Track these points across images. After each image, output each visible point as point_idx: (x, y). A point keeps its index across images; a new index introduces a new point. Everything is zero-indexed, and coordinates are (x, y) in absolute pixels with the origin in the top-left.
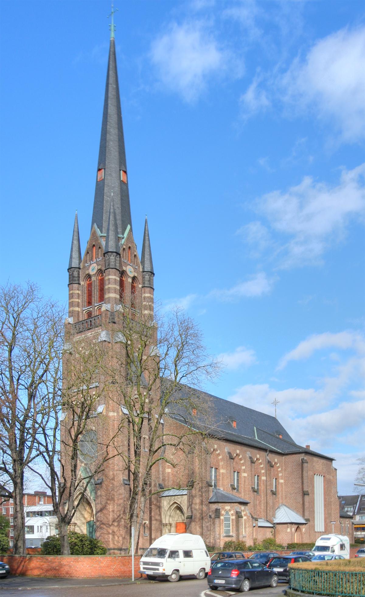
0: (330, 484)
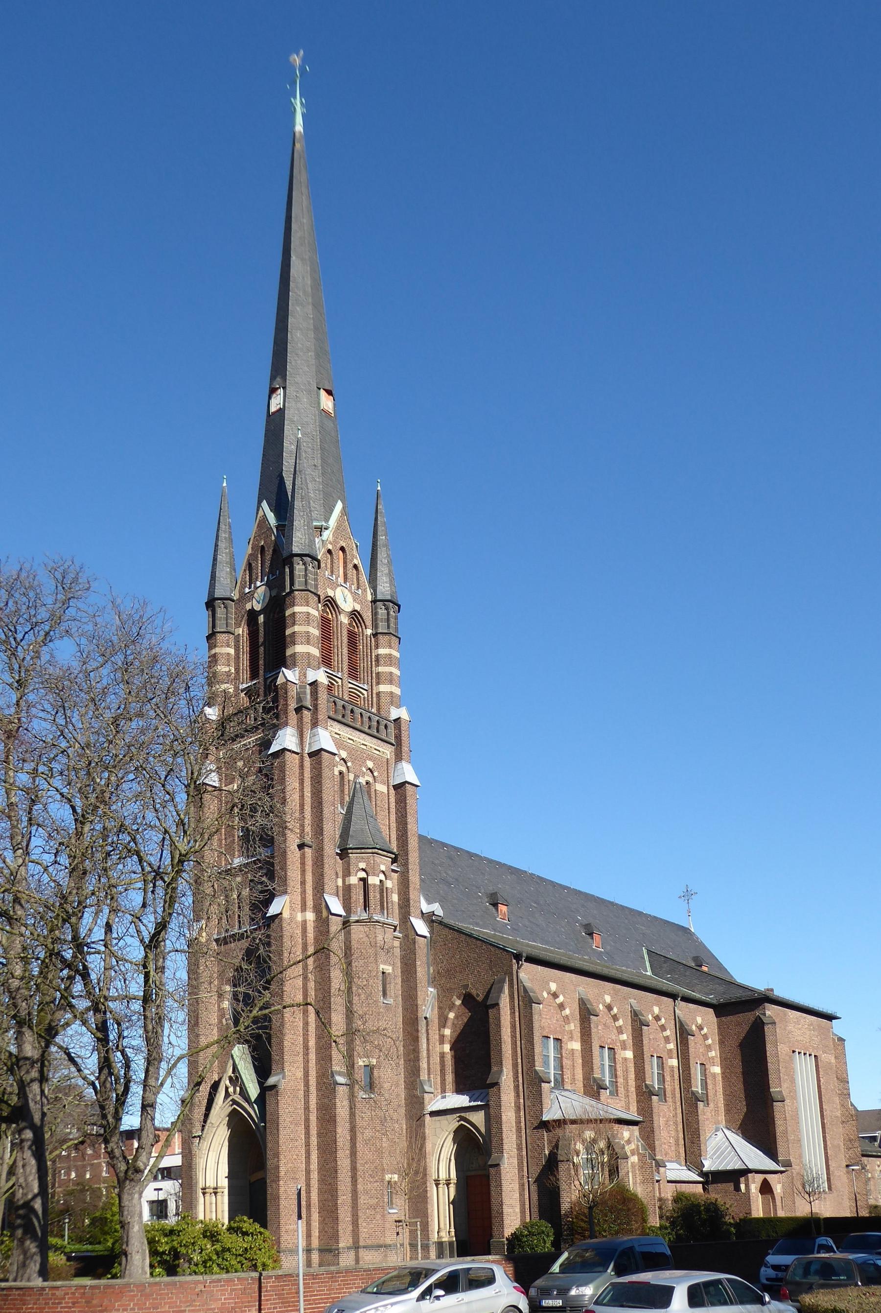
0: (834, 1079)
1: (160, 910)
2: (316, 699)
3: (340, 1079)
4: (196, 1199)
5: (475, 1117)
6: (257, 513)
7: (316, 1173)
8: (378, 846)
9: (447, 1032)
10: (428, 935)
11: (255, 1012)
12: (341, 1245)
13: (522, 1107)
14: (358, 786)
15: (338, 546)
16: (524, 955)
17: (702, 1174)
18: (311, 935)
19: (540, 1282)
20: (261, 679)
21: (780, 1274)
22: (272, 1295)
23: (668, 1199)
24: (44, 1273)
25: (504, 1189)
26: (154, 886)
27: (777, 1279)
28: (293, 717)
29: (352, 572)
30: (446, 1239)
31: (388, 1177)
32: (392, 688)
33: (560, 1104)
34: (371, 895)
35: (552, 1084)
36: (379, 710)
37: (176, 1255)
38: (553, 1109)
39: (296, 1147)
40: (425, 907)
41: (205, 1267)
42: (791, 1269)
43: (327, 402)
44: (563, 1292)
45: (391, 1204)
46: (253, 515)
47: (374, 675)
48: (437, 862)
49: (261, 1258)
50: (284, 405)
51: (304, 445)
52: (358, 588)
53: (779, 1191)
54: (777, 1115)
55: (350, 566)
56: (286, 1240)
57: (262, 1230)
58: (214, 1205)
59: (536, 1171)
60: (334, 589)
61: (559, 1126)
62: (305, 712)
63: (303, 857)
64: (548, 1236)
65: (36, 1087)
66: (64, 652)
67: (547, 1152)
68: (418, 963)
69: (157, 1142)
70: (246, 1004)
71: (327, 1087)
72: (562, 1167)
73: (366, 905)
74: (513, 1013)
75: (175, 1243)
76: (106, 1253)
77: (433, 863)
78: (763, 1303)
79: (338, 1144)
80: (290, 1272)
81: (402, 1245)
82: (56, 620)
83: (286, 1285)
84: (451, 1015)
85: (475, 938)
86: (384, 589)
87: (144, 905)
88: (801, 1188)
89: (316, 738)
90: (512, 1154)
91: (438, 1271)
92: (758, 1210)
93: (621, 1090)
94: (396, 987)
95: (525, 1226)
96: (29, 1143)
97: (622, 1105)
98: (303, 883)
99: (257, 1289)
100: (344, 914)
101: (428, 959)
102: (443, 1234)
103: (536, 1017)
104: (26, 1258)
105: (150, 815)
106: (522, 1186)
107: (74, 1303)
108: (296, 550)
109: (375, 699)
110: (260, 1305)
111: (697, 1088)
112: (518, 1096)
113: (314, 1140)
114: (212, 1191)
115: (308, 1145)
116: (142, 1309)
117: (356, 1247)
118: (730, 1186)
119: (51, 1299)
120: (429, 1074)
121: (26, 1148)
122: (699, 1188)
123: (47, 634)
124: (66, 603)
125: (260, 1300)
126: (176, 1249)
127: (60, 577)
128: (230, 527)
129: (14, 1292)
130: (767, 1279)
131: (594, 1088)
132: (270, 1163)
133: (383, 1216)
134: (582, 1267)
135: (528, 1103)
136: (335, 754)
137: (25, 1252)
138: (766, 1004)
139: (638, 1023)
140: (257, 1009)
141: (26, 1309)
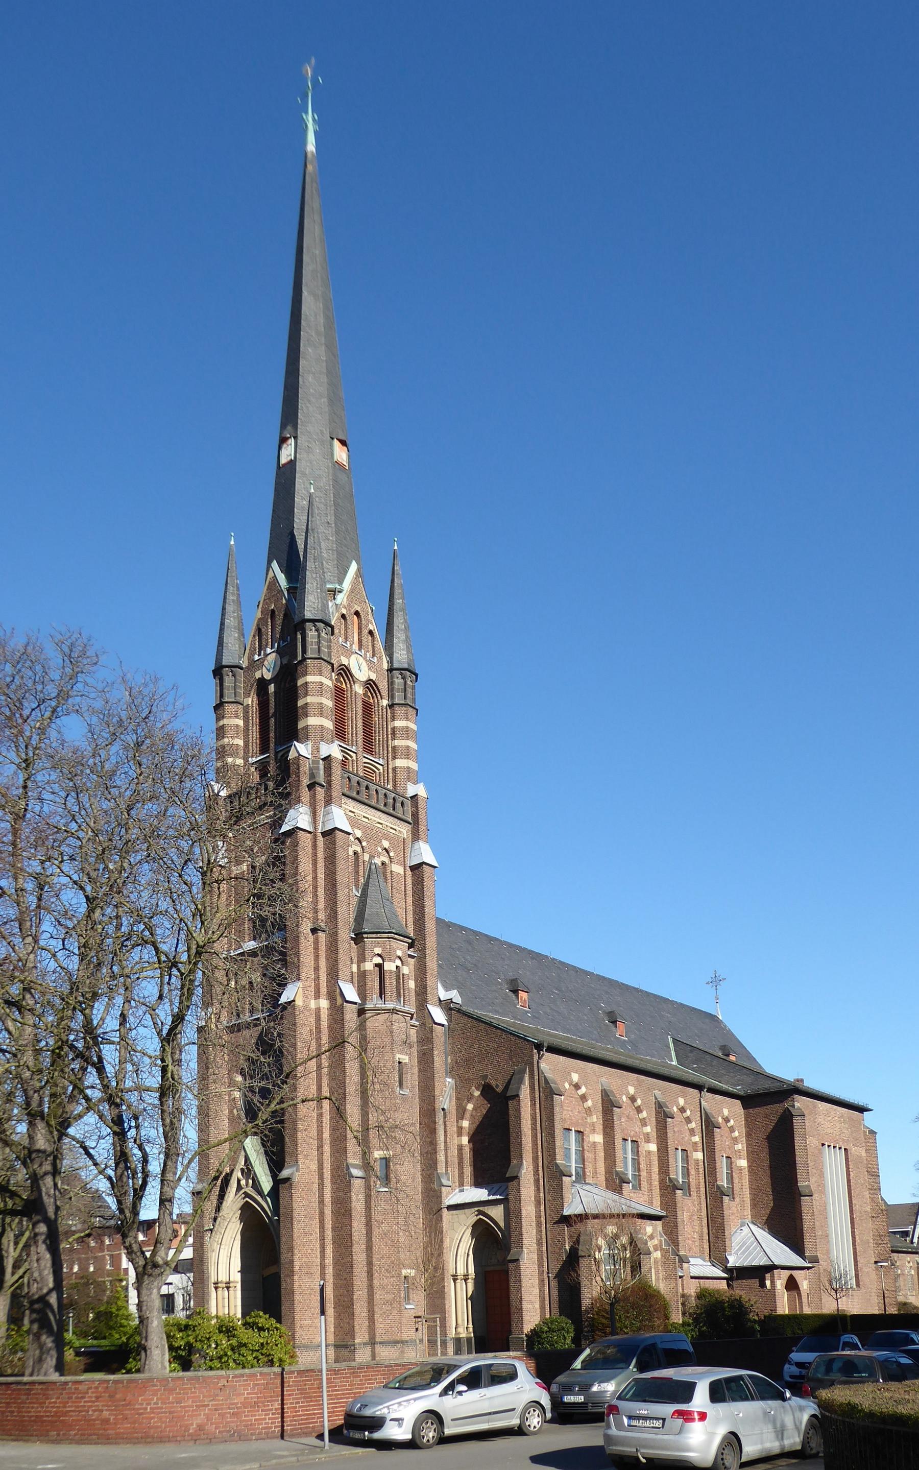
0: (864, 1172)
1: (177, 1002)
2: (330, 775)
3: (355, 1172)
4: (208, 1294)
5: (494, 1211)
6: (267, 574)
7: (331, 1268)
8: (394, 931)
9: (465, 1124)
10: (446, 1023)
11: (273, 1107)
12: (356, 1341)
13: (542, 1201)
14: (373, 867)
15: (353, 611)
16: (546, 1044)
17: (727, 1270)
18: (325, 1023)
19: (561, 1378)
20: (272, 753)
21: (804, 1372)
22: (294, 1390)
23: (690, 1296)
24: (60, 1367)
25: (523, 1284)
26: (170, 975)
27: (801, 1377)
28: (305, 794)
29: (367, 639)
30: (463, 1335)
31: (404, 1272)
32: (409, 767)
33: (582, 1198)
34: (387, 981)
35: (574, 1178)
36: (395, 786)
37: (190, 1347)
38: (574, 1203)
39: (311, 1241)
40: (443, 994)
41: (221, 1362)
42: (813, 1366)
43: (341, 454)
44: (585, 1388)
45: (408, 1299)
46: (262, 576)
47: (390, 749)
48: (455, 946)
49: (277, 1354)
50: (295, 457)
51: (316, 502)
52: (373, 656)
53: (805, 1287)
54: (805, 1210)
55: (365, 632)
56: (301, 1335)
57: (278, 1325)
58: (226, 1300)
59: (556, 1267)
60: (348, 657)
61: (581, 1221)
62: (318, 789)
63: (316, 942)
64: (568, 1333)
65: (49, 1180)
66: (73, 731)
67: (568, 1248)
68: (436, 1053)
69: (176, 1236)
70: (264, 1097)
71: (342, 1179)
72: (583, 1262)
73: (382, 993)
74: (533, 1105)
75: (191, 1339)
76: (113, 1348)
77: (451, 947)
78: (784, 1399)
79: (354, 1238)
80: (312, 1367)
81: (421, 1341)
82: (63, 696)
83: (307, 1381)
84: (470, 1107)
85: (495, 1027)
86: (401, 656)
87: (161, 997)
88: (827, 1284)
89: (329, 817)
90: (532, 1249)
91: (460, 1367)
92: (783, 1307)
93: (644, 1184)
94: (413, 1077)
95: (544, 1322)
96: (43, 1237)
97: (644, 1199)
98: (317, 969)
99: (279, 1385)
100: (359, 1001)
101: (446, 1048)
102: (460, 1330)
103: (557, 1109)
104: (42, 1353)
105: (164, 905)
106: (542, 1281)
107: (97, 1398)
108: (308, 615)
109: (391, 775)
110: (282, 1400)
111: (723, 1182)
112: (538, 1189)
113: (329, 1234)
114: (224, 1285)
115: (322, 1239)
116: (165, 1403)
117: (372, 1342)
118: (755, 1282)
119: (74, 1393)
120: (446, 1167)
121: (40, 1242)
122: (723, 1285)
123: (54, 711)
124: (73, 677)
125: (283, 1395)
126: (192, 1345)
127: (67, 650)
128: (238, 589)
129: (37, 1386)
130: (791, 1377)
131: (616, 1182)
132: (284, 1257)
133: (400, 1311)
134: (605, 1364)
135: (548, 1197)
136: (349, 834)
137: (41, 1346)
138: (796, 1096)
139: (663, 1115)
140: (275, 1103)
141: (50, 1403)
